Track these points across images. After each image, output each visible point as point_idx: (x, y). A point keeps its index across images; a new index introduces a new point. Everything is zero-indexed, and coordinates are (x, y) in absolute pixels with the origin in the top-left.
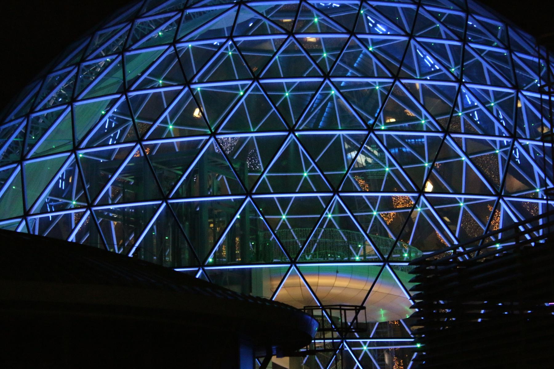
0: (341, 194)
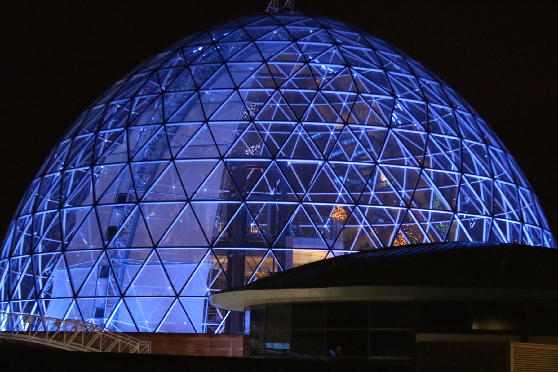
0: (304, 203)
